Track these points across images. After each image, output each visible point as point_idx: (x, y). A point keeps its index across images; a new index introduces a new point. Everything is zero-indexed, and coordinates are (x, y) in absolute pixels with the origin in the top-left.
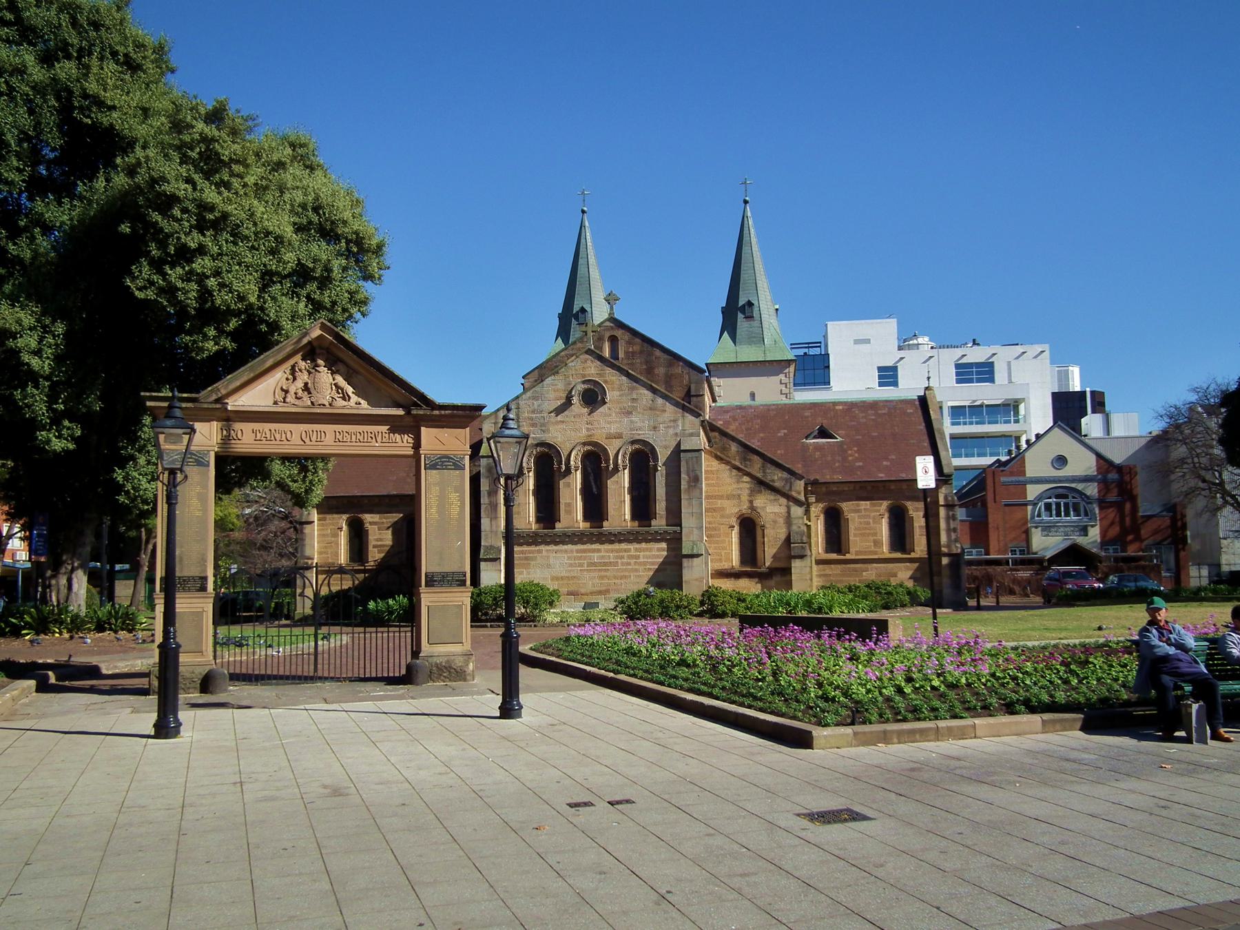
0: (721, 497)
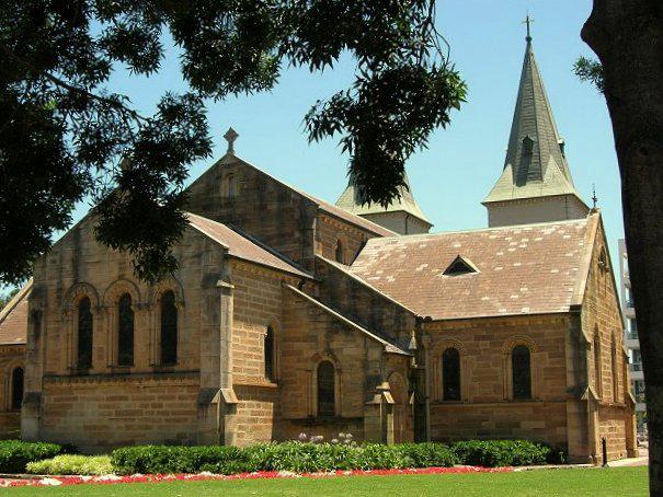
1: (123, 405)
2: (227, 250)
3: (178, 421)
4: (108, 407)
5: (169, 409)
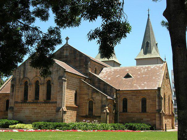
0: (84, 95)
1: (36, 111)
3: (50, 115)
4: (32, 111)
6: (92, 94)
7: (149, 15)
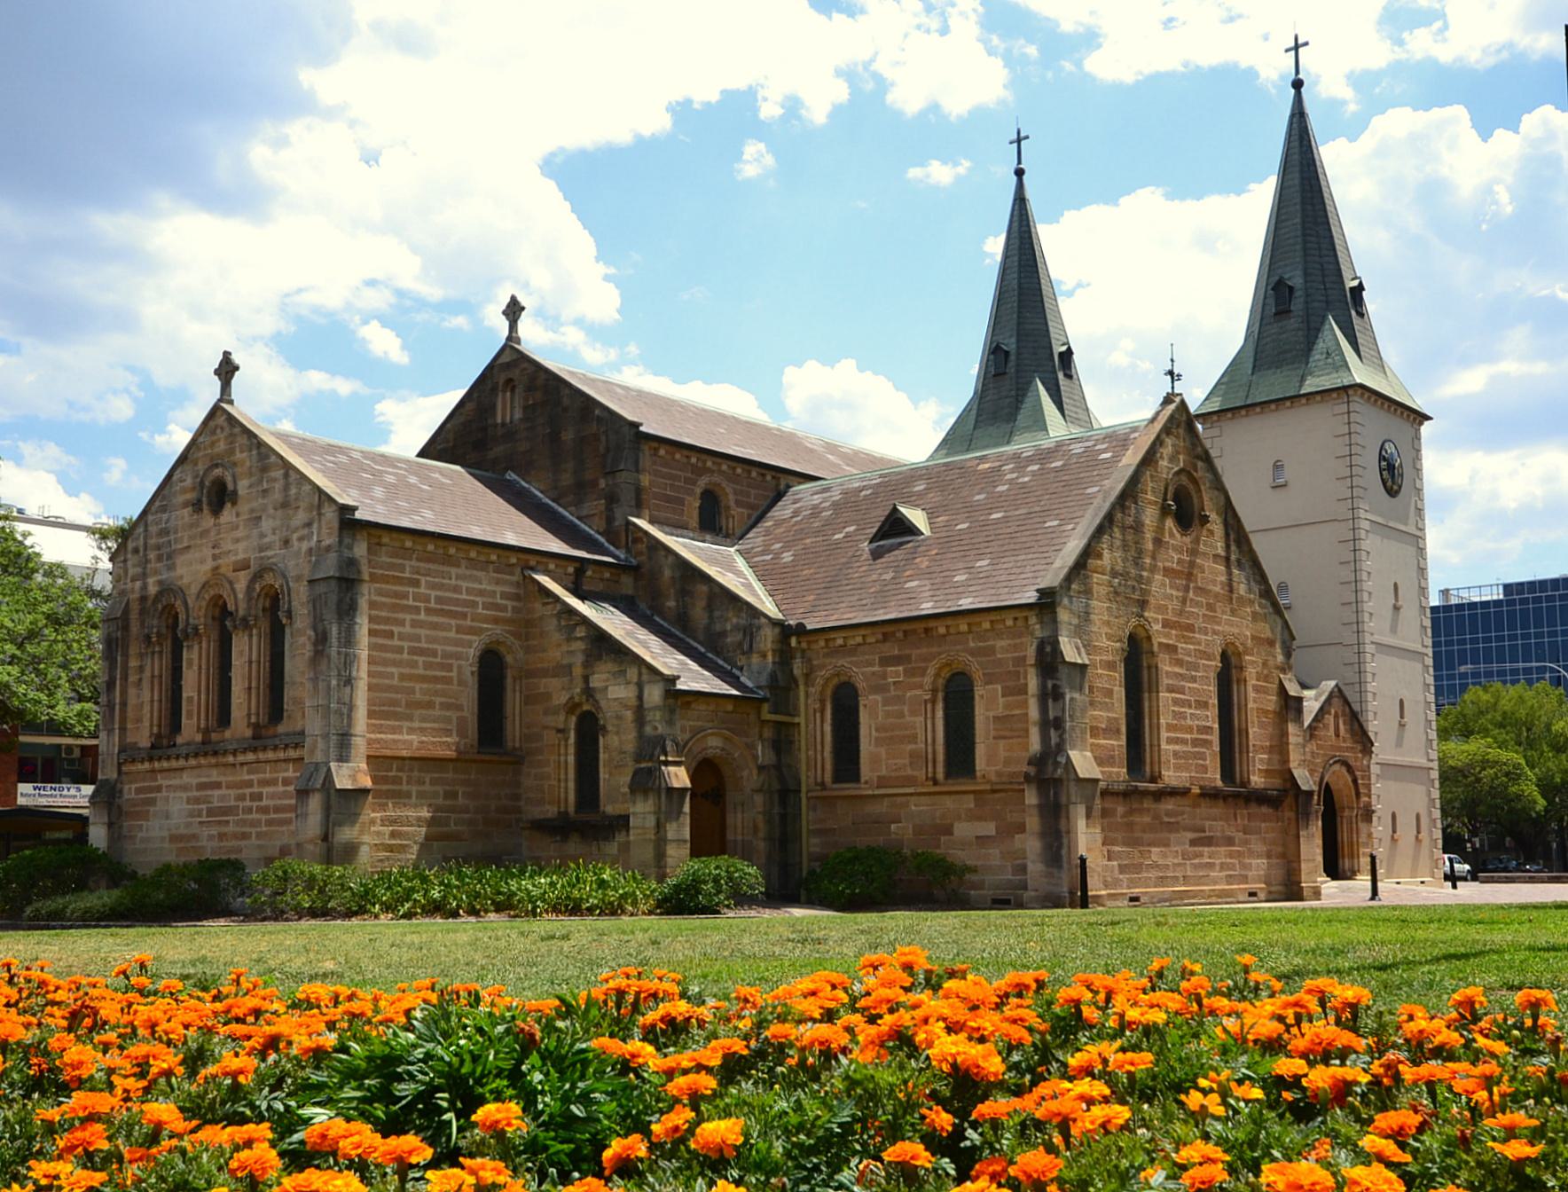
2: (353, 509)
5: (271, 803)
6: (588, 664)
7: (1019, 173)
